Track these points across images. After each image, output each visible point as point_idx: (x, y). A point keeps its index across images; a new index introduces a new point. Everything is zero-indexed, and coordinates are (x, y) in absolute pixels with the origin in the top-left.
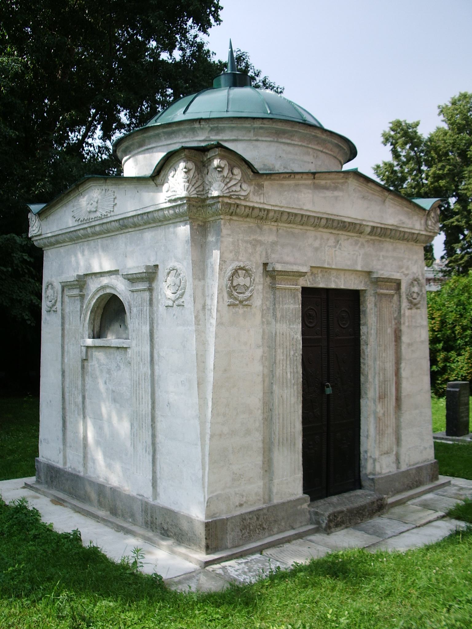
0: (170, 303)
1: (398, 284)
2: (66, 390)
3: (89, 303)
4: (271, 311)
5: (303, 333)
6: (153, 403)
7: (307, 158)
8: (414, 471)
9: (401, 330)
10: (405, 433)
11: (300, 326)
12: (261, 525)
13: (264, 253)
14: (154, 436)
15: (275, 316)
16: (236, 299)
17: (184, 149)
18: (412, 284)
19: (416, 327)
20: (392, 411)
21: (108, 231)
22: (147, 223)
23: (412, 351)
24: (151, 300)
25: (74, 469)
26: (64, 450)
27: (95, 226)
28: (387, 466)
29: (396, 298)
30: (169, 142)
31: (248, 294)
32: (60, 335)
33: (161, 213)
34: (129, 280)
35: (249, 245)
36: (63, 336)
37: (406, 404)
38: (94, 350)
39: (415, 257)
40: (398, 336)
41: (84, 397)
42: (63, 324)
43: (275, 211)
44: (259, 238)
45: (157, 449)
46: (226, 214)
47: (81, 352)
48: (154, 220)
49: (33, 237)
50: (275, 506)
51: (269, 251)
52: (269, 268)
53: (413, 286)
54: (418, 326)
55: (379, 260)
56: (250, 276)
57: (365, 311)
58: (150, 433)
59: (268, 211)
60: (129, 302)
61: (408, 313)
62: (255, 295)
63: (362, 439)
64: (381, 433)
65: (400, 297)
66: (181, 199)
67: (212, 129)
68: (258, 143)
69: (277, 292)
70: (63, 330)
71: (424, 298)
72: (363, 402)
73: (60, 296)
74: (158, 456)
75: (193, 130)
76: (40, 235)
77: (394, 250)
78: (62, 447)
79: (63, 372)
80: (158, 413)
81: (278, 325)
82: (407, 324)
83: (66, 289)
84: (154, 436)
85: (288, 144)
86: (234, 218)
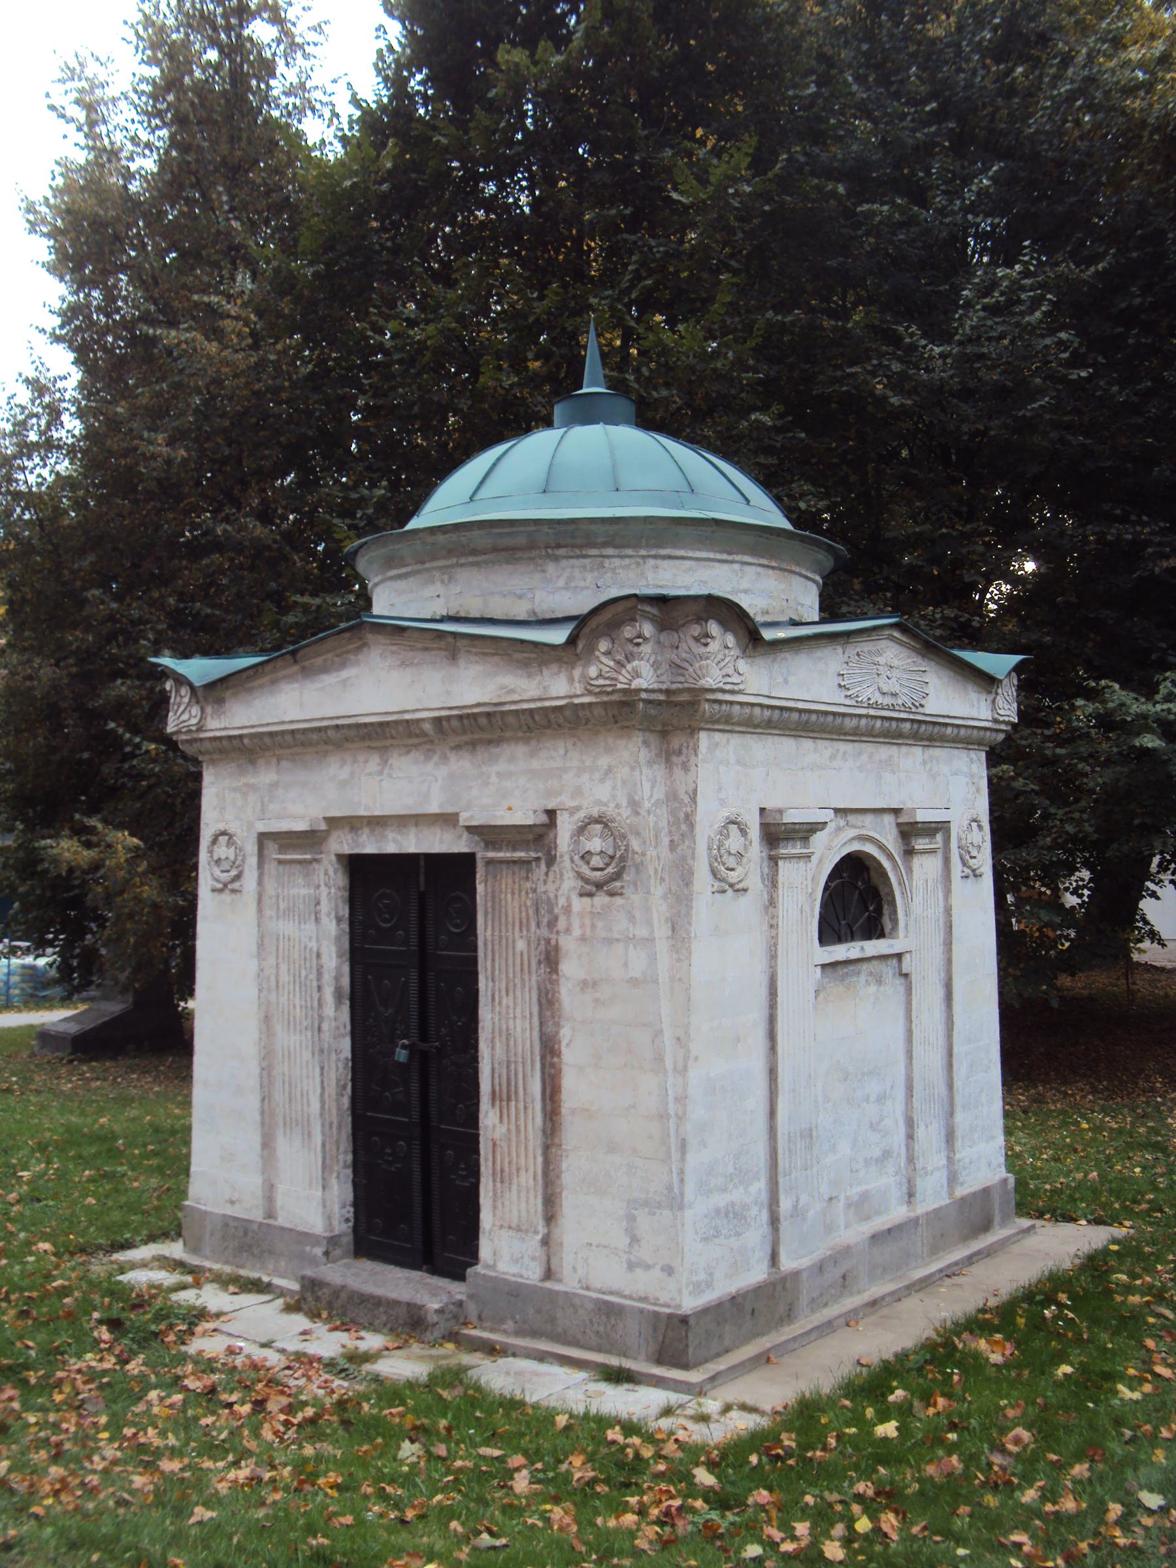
7: (430, 591)
8: (590, 1306)
12: (250, 1246)
19: (610, 941)
23: (597, 1000)
35: (238, 795)
37: (573, 1131)
39: (604, 761)
40: (551, 959)
44: (252, 781)
54: (618, 940)
61: (578, 904)
69: (780, 863)
77: (533, 754)
82: (577, 932)
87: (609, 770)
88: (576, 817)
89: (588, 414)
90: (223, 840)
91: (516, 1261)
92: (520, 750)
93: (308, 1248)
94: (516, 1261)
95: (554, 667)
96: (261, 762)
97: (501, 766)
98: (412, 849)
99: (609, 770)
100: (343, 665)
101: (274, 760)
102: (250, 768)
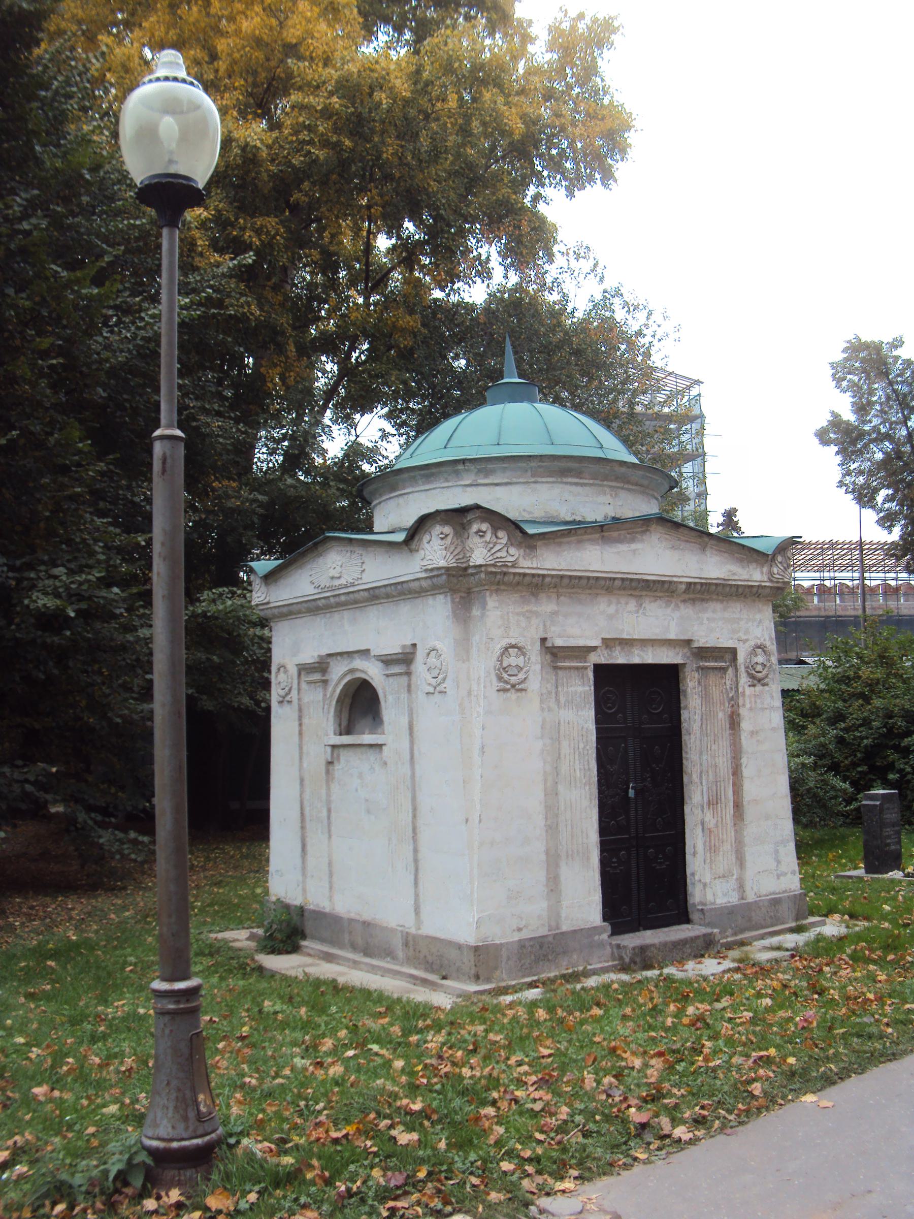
0: (431, 690)
1: (733, 652)
2: (306, 803)
3: (334, 691)
4: (554, 695)
5: (598, 721)
6: (415, 810)
8: (766, 904)
9: (739, 715)
10: (750, 852)
11: (592, 713)
12: (545, 956)
13: (541, 626)
14: (416, 851)
15: (558, 701)
16: (506, 682)
17: (438, 512)
18: (753, 653)
19: (763, 709)
20: (729, 822)
21: (356, 602)
22: (401, 593)
24: (409, 686)
25: (317, 905)
26: (304, 882)
27: (339, 595)
28: (725, 895)
29: (730, 671)
30: (427, 487)
31: (521, 676)
32: (297, 732)
33: (416, 584)
34: (382, 661)
35: (522, 618)
36: (301, 733)
37: (750, 812)
38: (341, 750)
39: (758, 616)
40: (734, 722)
41: (329, 811)
42: (300, 718)
43: (553, 576)
45: (420, 867)
46: (492, 583)
47: (326, 752)
48: (410, 592)
49: (257, 605)
50: (562, 933)
51: (548, 623)
52: (549, 644)
53: (756, 655)
55: (702, 624)
56: (524, 654)
57: (685, 691)
58: (411, 848)
59: (544, 576)
60: (383, 689)
61: (749, 691)
62: (531, 677)
63: (689, 858)
64: (712, 849)
65: (736, 670)
66: (439, 569)
67: (480, 471)
68: (538, 486)
70: (300, 725)
71: (774, 671)
72: (687, 809)
73: (295, 682)
74: (420, 875)
75: (457, 473)
76: (268, 603)
77: (725, 609)
78: (300, 878)
79: (302, 781)
80: (420, 822)
81: (562, 711)
82: (748, 706)
83: (303, 673)
84: (416, 851)
85: (576, 484)
86: (502, 587)
87: (760, 621)
88: (747, 644)
89: (515, 395)
90: (433, 653)
91: (725, 895)
92: (718, 606)
93: (596, 938)
94: (725, 895)
95: (754, 565)
96: (542, 596)
97: (709, 614)
98: (650, 661)
99: (760, 621)
100: (633, 540)
101: (554, 596)
102: (533, 600)
